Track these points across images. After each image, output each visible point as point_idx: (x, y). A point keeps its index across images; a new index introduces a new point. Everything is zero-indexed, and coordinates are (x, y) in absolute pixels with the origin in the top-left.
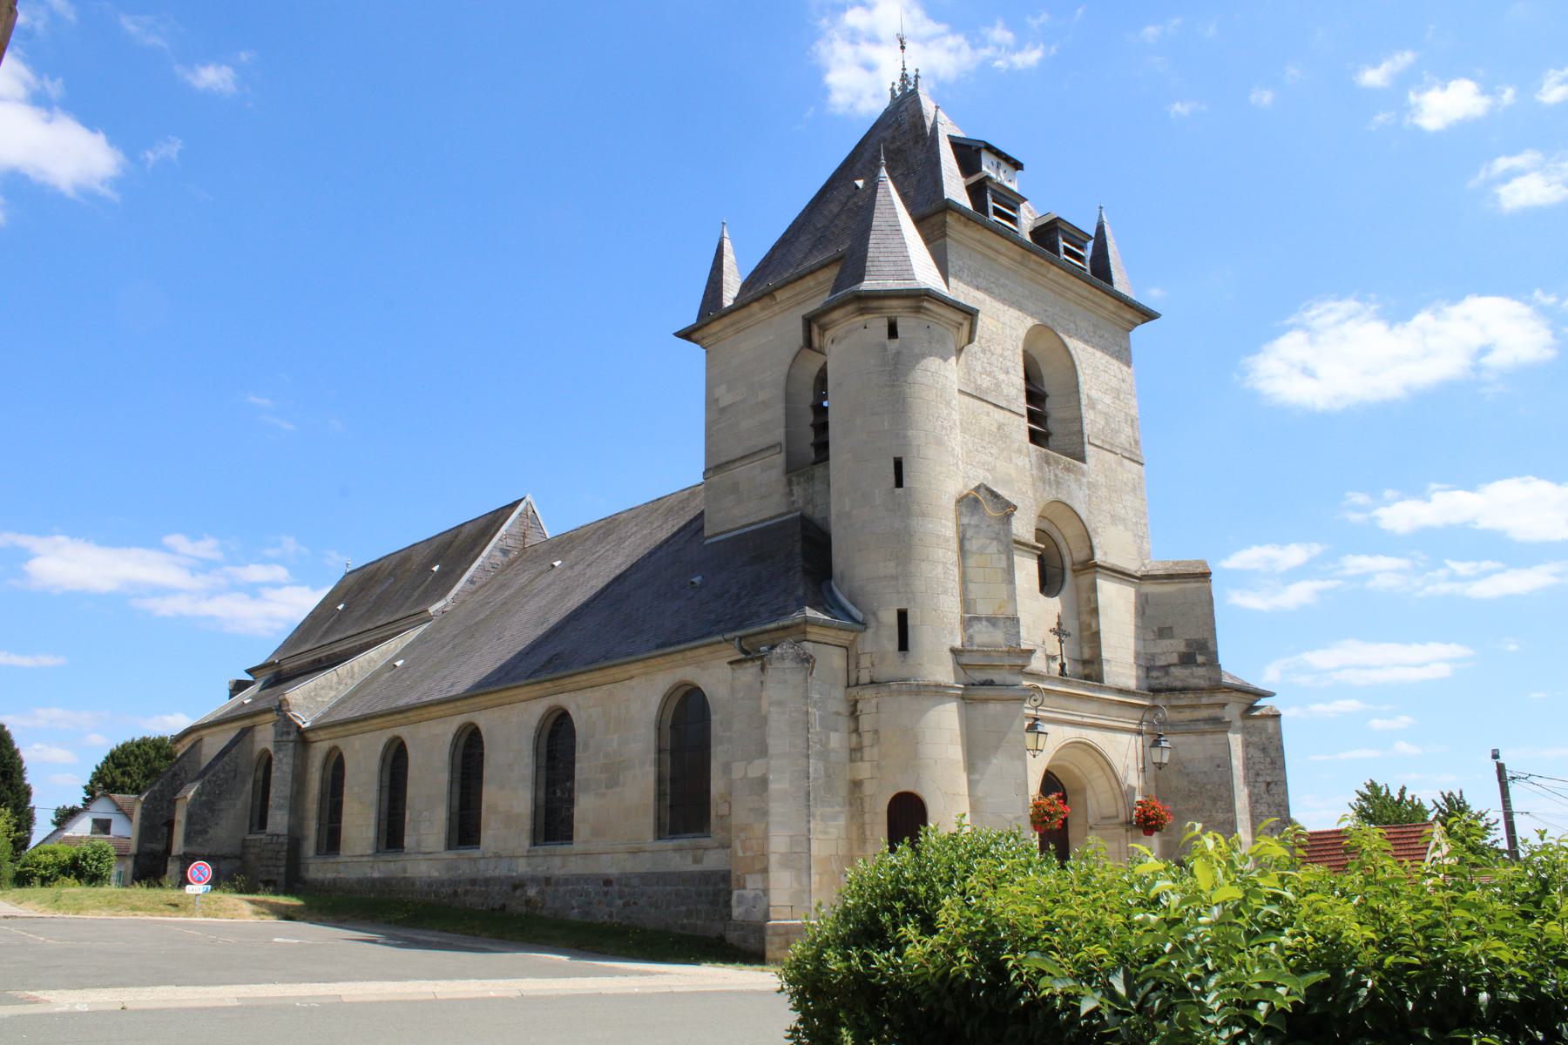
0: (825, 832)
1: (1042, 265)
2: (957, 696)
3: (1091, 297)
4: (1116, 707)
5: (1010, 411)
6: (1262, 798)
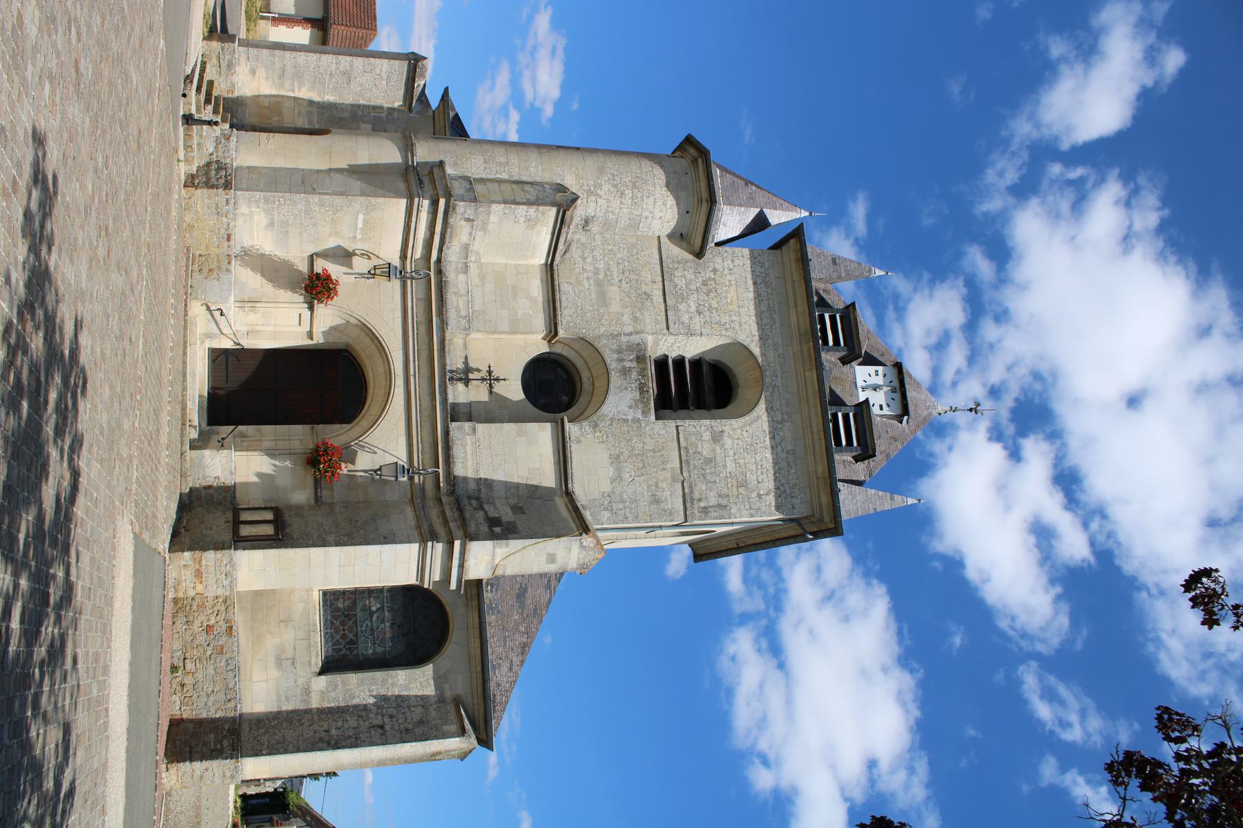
0: (299, 114)
1: (811, 360)
2: (407, 162)
3: (816, 437)
4: (431, 440)
5: (666, 311)
6: (364, 721)
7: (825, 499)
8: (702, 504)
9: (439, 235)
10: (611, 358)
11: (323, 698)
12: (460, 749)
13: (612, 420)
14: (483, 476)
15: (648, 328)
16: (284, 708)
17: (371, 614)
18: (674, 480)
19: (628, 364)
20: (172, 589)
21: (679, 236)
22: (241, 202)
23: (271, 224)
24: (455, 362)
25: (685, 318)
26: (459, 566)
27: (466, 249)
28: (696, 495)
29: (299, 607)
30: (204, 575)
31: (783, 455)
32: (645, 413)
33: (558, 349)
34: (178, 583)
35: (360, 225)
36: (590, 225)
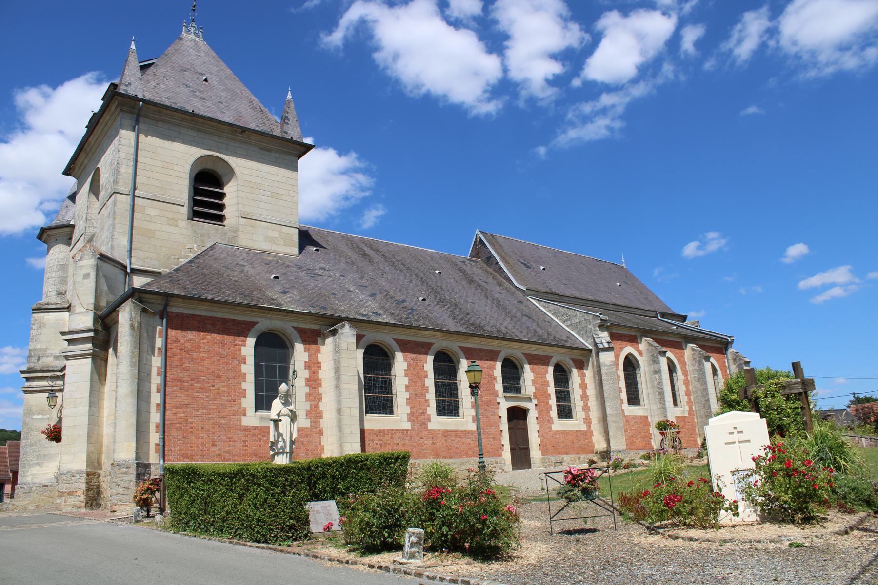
12: (131, 310)
20: (79, 510)
21: (68, 241)
22: (24, 481)
23: (39, 464)
26: (78, 334)
30: (71, 490)
34: (74, 506)
35: (41, 416)
36: (61, 291)
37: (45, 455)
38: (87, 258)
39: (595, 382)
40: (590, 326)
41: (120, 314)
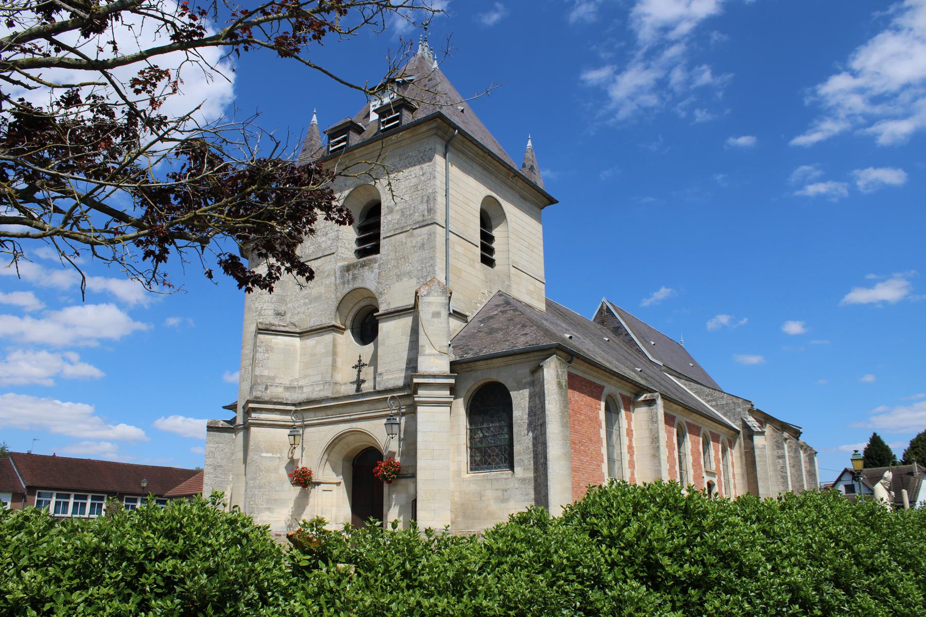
7: (424, 128)
8: (426, 213)
9: (277, 405)
10: (347, 289)
11: (528, 469)
12: (557, 367)
13: (379, 283)
14: (405, 366)
15: (333, 266)
16: (533, 496)
17: (485, 437)
18: (412, 235)
19: (351, 277)
23: (269, 509)
24: (351, 390)
25: (329, 242)
27: (287, 388)
28: (421, 219)
29: (473, 487)
31: (402, 162)
32: (375, 261)
33: (349, 323)
35: (270, 455)
37: (275, 500)
38: (436, 294)
39: (742, 462)
40: (739, 410)
41: (545, 370)
